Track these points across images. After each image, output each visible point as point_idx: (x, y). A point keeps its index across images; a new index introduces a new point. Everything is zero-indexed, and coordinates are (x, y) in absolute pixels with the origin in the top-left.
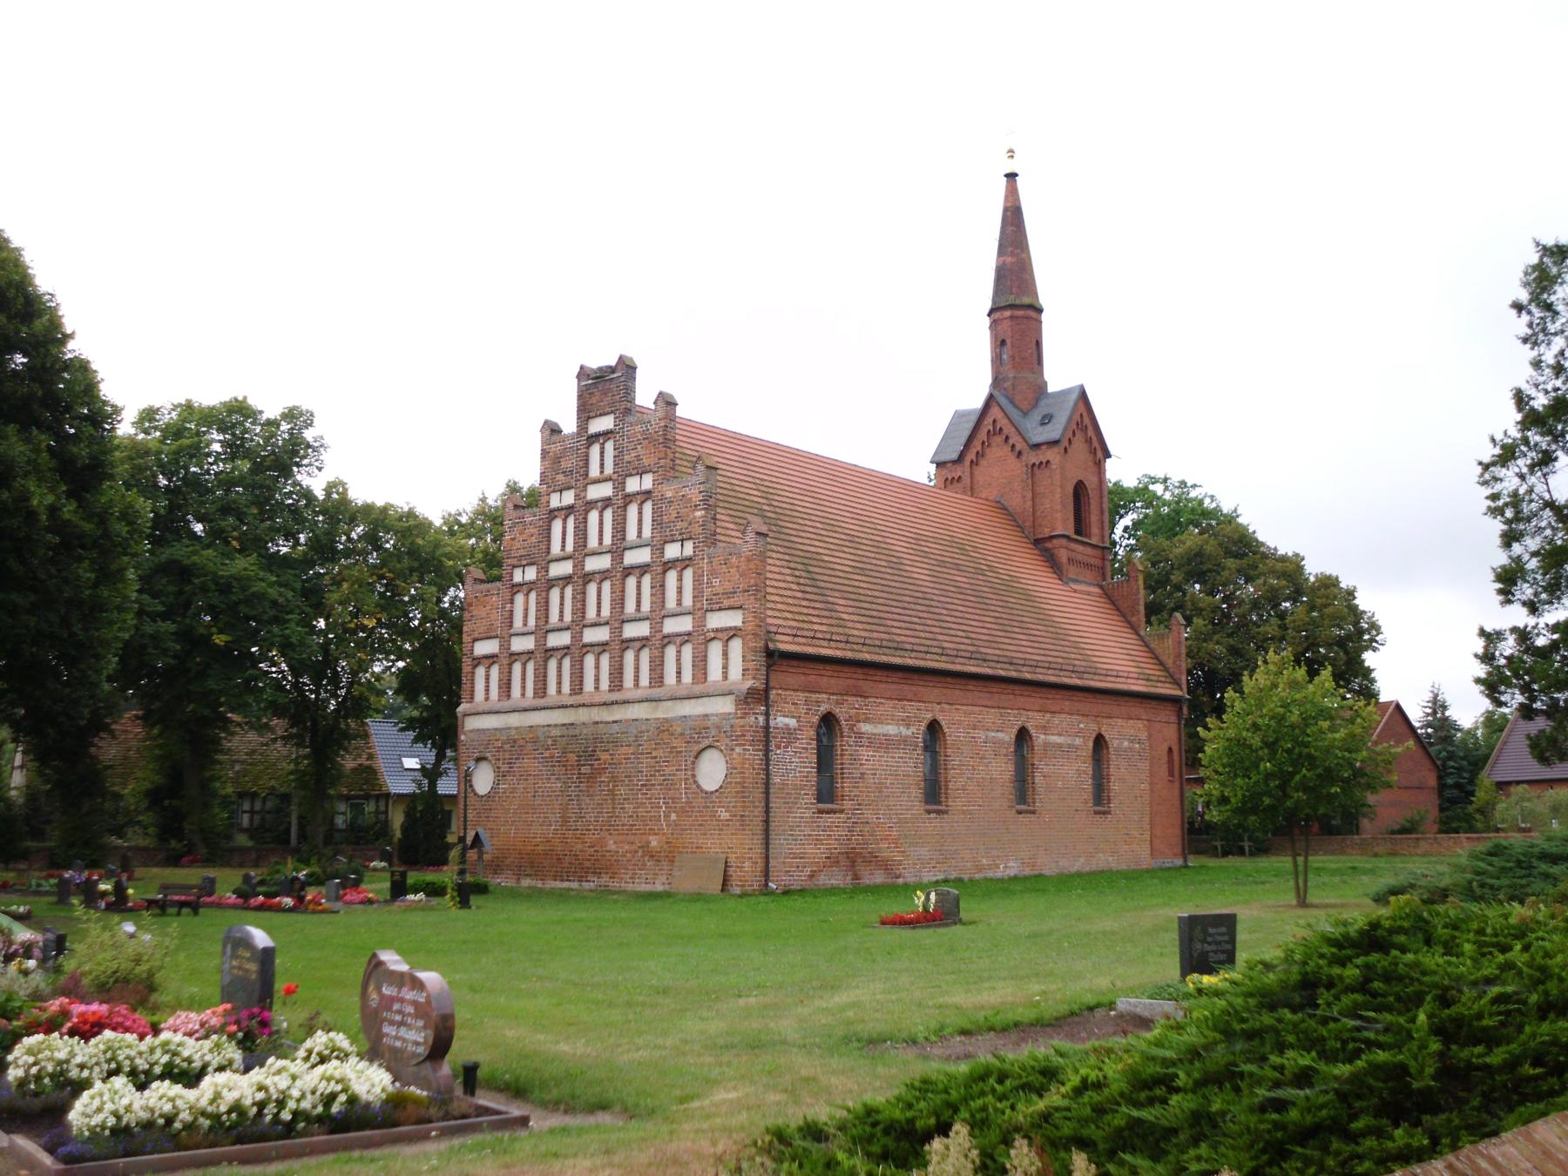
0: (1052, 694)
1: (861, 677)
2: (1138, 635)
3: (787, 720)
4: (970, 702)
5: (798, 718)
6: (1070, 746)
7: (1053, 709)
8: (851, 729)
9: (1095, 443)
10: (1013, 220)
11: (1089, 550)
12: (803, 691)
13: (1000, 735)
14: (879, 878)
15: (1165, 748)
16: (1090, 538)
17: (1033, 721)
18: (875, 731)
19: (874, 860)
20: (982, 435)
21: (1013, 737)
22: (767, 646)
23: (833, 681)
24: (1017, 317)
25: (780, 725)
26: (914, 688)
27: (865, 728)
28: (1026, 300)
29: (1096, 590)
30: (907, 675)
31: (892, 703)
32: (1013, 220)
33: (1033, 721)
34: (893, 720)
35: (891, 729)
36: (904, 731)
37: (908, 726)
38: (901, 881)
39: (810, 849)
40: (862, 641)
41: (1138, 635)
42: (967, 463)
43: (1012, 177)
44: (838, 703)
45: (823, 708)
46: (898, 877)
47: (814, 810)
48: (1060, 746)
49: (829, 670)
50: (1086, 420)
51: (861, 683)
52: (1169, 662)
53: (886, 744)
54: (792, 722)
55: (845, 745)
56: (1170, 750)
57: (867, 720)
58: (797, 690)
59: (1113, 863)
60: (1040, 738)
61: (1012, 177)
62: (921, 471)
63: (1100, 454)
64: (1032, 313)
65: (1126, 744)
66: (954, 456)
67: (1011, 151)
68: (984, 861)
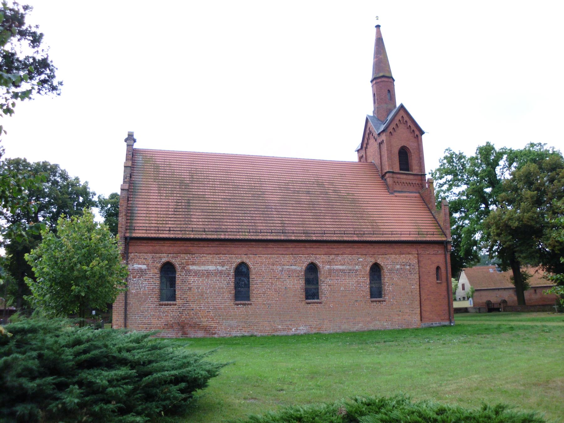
0: (332, 245)
1: (190, 245)
2: (431, 213)
3: (140, 266)
4: (269, 253)
5: (148, 265)
6: (350, 270)
7: (336, 253)
8: (183, 268)
9: (413, 127)
10: (379, 43)
11: (411, 177)
12: (151, 253)
13: (293, 267)
14: (200, 334)
15: (434, 267)
16: (412, 171)
17: (320, 260)
18: (199, 269)
19: (196, 326)
20: (367, 136)
21: (304, 268)
22: (125, 235)
23: (170, 248)
24: (378, 82)
25: (136, 268)
26: (228, 249)
27: (191, 267)
28: (387, 75)
29: (417, 195)
30: (222, 243)
31: (211, 256)
32: (379, 43)
33: (320, 260)
34: (212, 263)
35: (211, 268)
36: (220, 268)
37: (223, 266)
38: (216, 336)
39: (154, 321)
40: (432, 233)
41: (431, 213)
42: (364, 148)
43: (378, 27)
44: (173, 257)
45: (164, 260)
46: (215, 334)
47: (157, 303)
48: (343, 271)
49: (168, 243)
50: (406, 118)
51: (190, 248)
52: (442, 224)
53: (142, 272)
54: (144, 267)
55: (179, 276)
56: (438, 268)
57: (193, 264)
58: (147, 253)
59: (387, 325)
60: (324, 268)
61: (378, 27)
62: (354, 158)
63: (417, 133)
64: (391, 80)
65: (398, 267)
66: (360, 147)
67: (377, 17)
68: (280, 327)
